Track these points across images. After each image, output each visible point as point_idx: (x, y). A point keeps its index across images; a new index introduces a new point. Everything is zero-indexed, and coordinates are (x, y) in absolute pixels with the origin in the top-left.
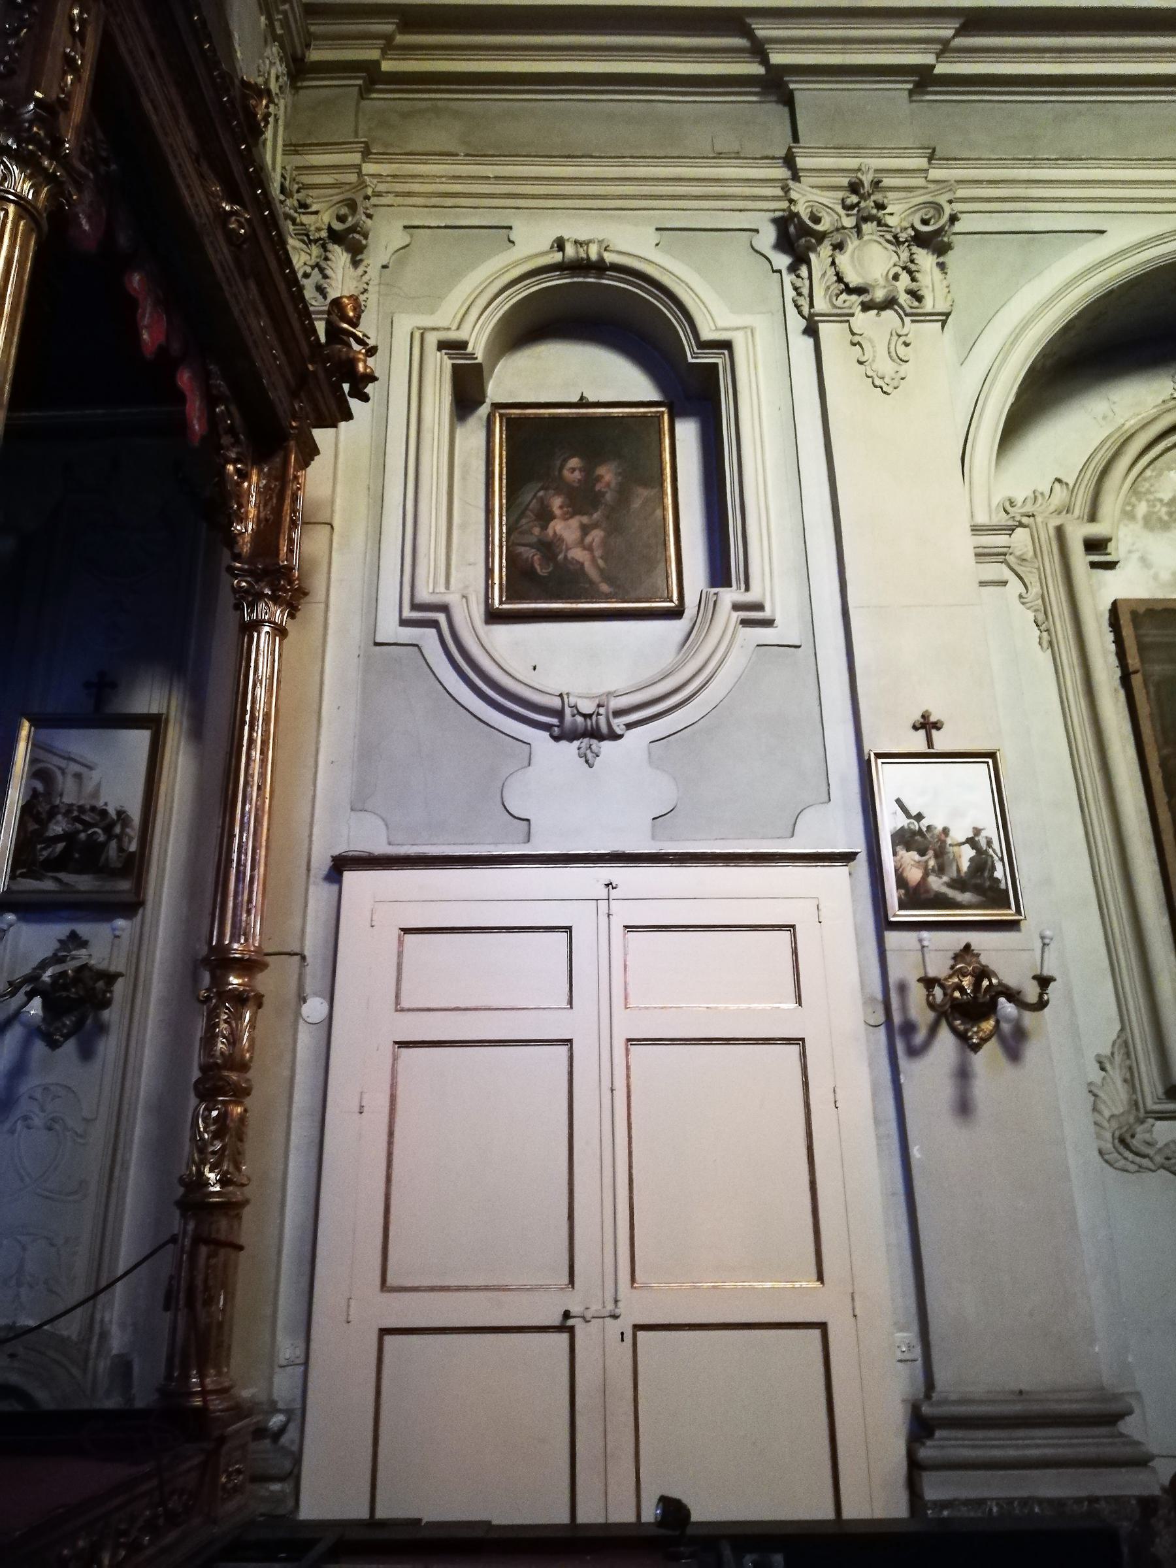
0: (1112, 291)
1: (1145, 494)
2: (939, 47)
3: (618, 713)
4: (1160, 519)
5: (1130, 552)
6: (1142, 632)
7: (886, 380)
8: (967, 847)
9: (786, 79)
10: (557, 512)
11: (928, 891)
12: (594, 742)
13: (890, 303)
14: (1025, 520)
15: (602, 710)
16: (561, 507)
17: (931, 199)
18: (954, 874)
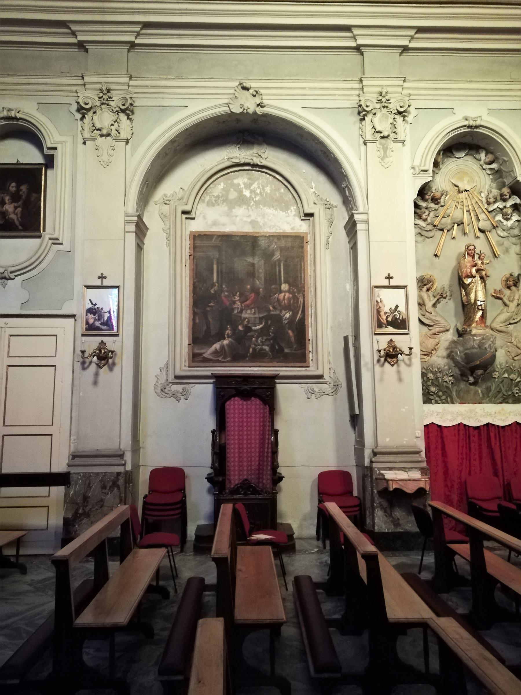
0: (187, 129)
1: (209, 193)
2: (136, 34)
3: (11, 272)
4: (212, 203)
5: (201, 214)
6: (196, 242)
7: (105, 163)
8: (108, 313)
9: (84, 45)
10: (7, 201)
11: (94, 326)
12: (5, 280)
13: (109, 135)
14: (168, 202)
15: (6, 272)
16: (8, 200)
17: (125, 96)
18: (102, 321)
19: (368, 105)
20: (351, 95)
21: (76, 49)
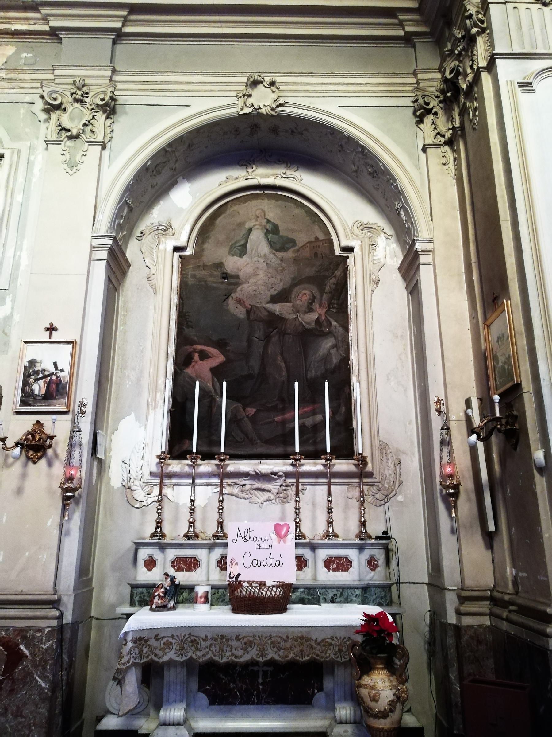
19: (54, 97)
20: (230, 91)
21: (403, 44)
